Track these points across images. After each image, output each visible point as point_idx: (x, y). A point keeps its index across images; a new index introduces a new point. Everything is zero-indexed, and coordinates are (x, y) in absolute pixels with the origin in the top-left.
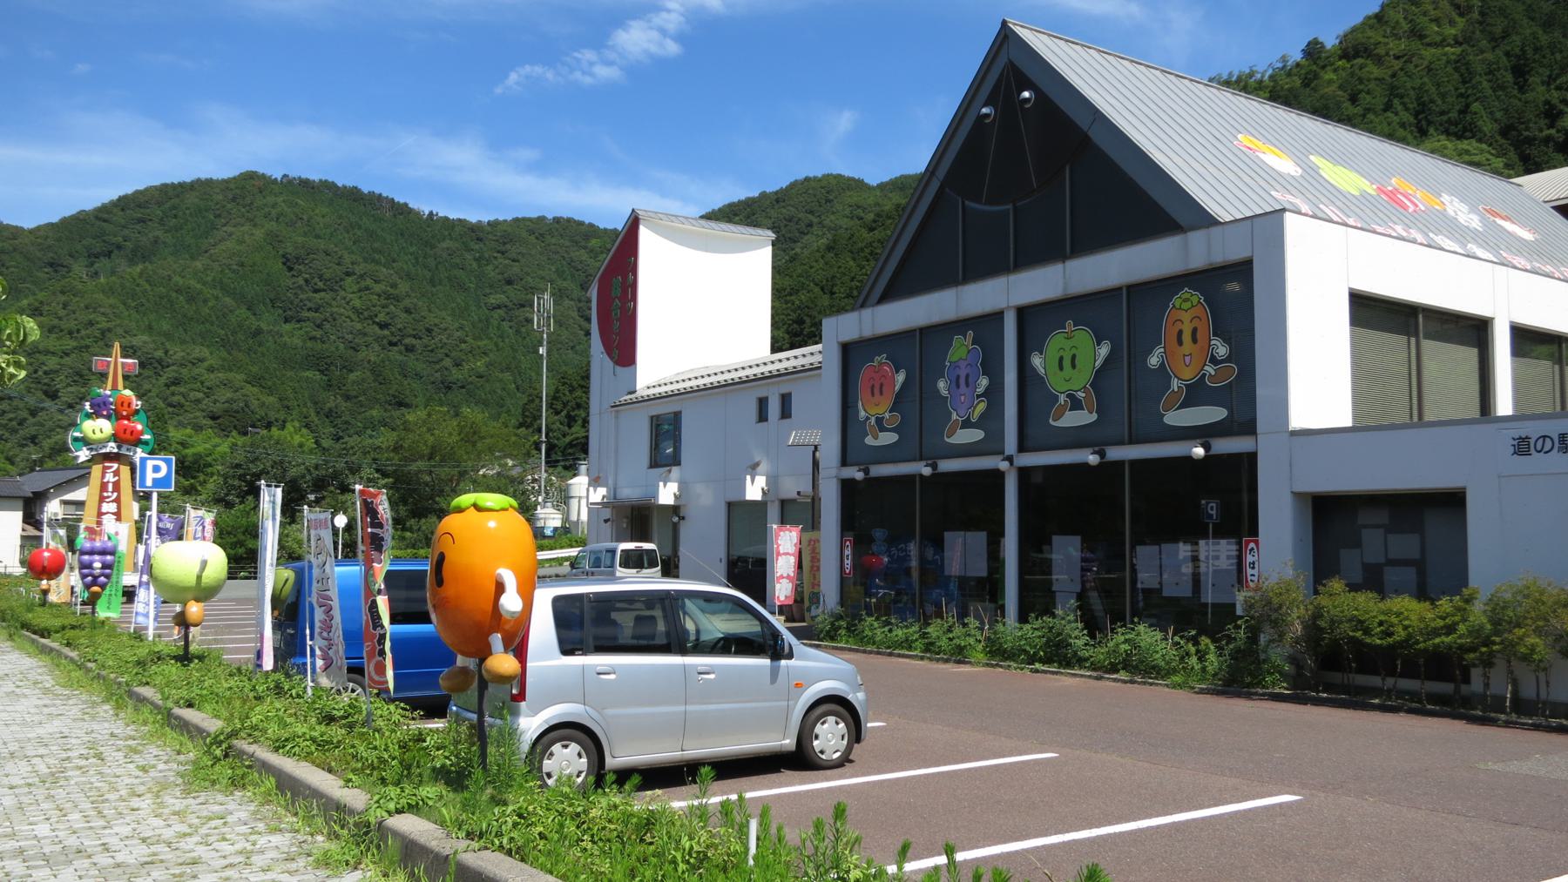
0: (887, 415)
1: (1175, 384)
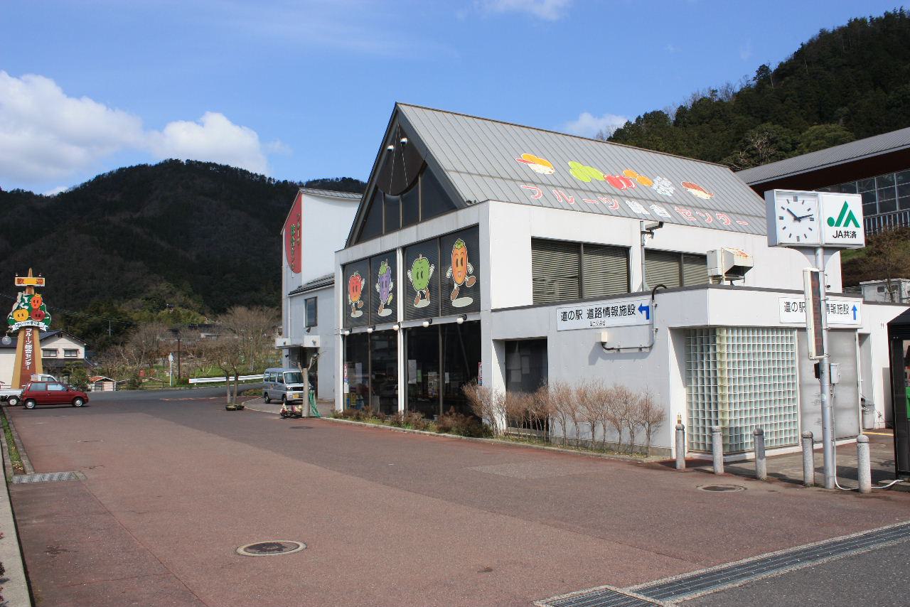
1: (456, 286)
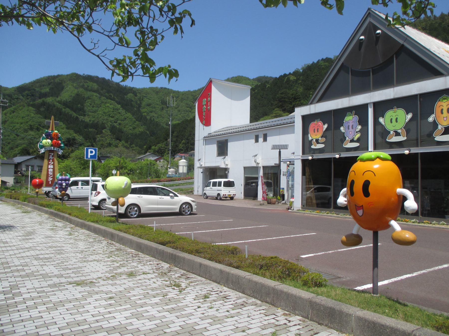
0: (320, 139)
1: (440, 127)
